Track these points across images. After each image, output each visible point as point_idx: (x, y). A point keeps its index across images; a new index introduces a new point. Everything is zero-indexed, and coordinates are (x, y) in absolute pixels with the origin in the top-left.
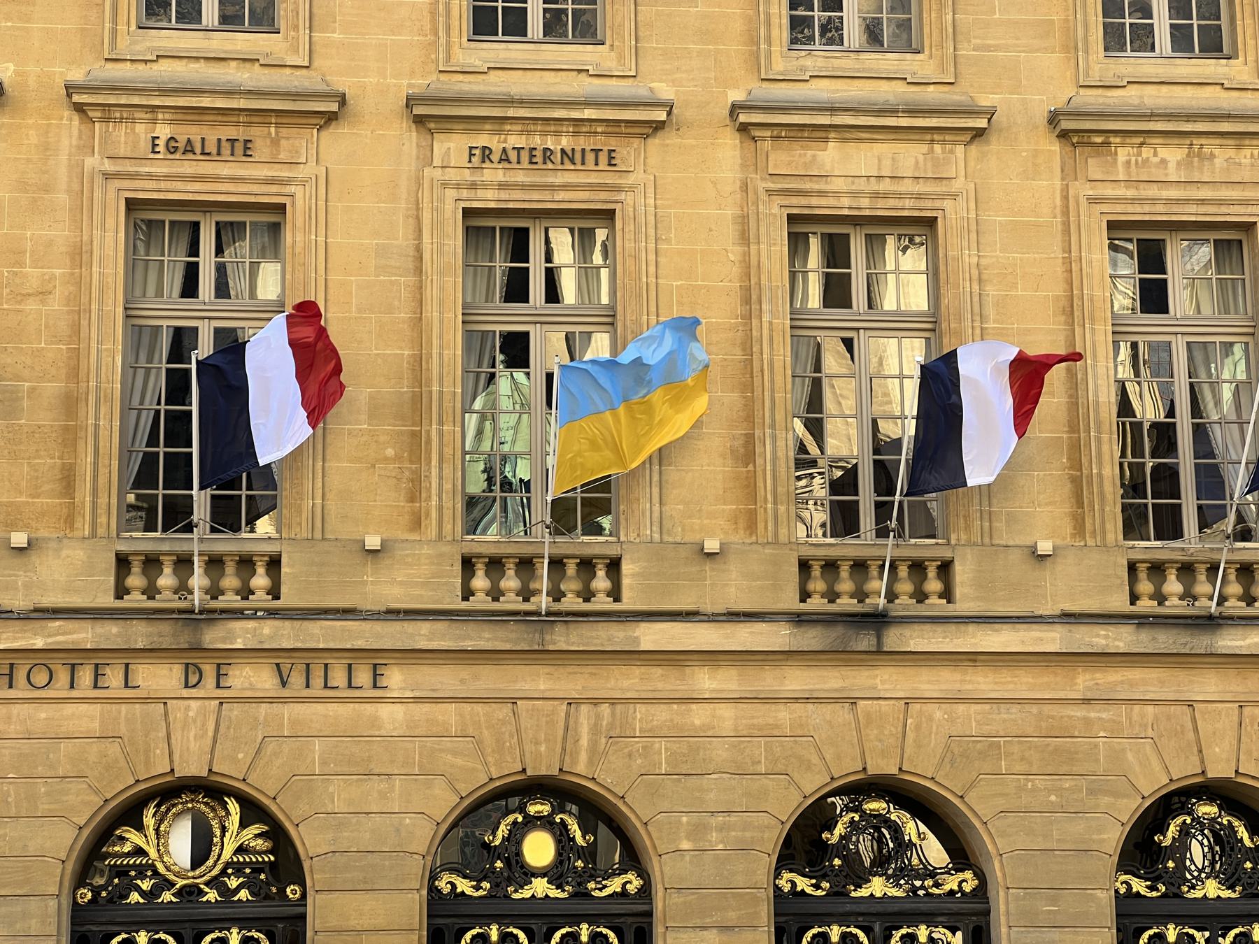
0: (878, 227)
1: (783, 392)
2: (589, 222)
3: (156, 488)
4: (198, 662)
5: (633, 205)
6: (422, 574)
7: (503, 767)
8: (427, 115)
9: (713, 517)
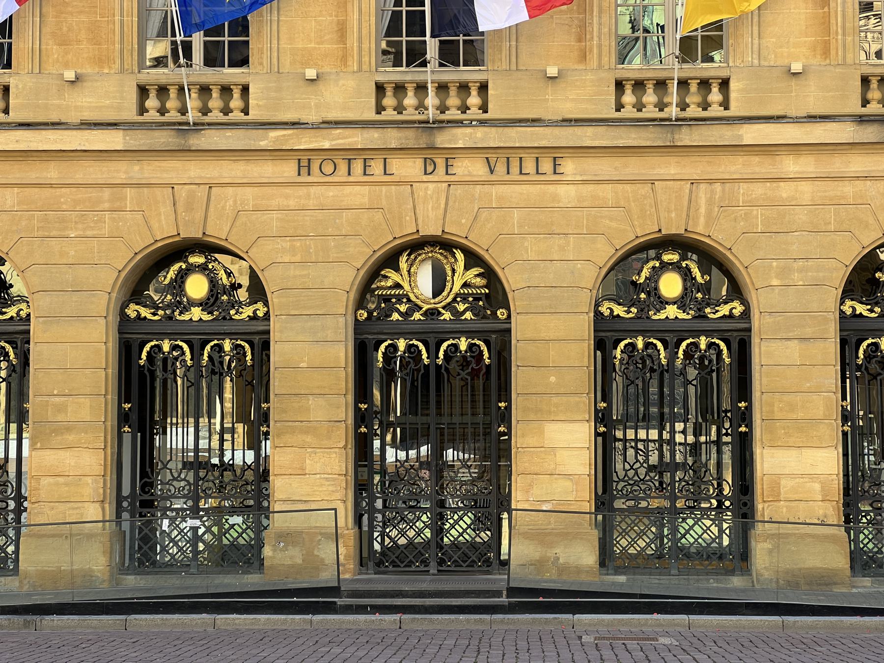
4: (432, 157)
6: (588, 93)
7: (646, 229)
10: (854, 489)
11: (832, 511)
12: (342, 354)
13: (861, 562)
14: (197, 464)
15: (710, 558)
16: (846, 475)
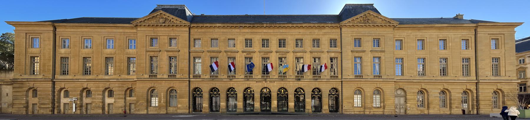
0: (300, 58)
1: (295, 67)
2: (285, 58)
3: (263, 72)
4: (266, 81)
5: (287, 57)
6: (277, 77)
7: (281, 87)
8: (243, 52)
9: (291, 74)
10: (295, 106)
11: (293, 107)
12: (259, 96)
13: (296, 111)
14: (249, 104)
15: (285, 110)
16: (5, 113)
